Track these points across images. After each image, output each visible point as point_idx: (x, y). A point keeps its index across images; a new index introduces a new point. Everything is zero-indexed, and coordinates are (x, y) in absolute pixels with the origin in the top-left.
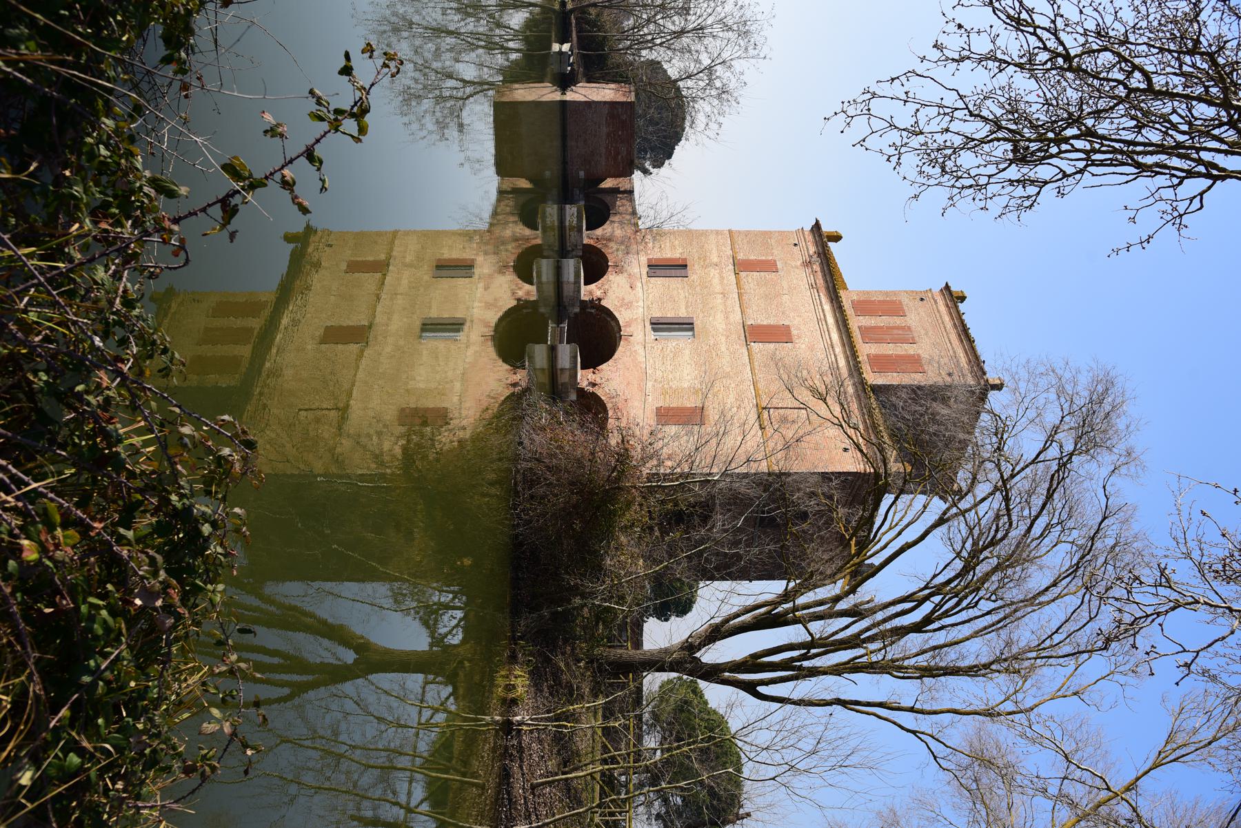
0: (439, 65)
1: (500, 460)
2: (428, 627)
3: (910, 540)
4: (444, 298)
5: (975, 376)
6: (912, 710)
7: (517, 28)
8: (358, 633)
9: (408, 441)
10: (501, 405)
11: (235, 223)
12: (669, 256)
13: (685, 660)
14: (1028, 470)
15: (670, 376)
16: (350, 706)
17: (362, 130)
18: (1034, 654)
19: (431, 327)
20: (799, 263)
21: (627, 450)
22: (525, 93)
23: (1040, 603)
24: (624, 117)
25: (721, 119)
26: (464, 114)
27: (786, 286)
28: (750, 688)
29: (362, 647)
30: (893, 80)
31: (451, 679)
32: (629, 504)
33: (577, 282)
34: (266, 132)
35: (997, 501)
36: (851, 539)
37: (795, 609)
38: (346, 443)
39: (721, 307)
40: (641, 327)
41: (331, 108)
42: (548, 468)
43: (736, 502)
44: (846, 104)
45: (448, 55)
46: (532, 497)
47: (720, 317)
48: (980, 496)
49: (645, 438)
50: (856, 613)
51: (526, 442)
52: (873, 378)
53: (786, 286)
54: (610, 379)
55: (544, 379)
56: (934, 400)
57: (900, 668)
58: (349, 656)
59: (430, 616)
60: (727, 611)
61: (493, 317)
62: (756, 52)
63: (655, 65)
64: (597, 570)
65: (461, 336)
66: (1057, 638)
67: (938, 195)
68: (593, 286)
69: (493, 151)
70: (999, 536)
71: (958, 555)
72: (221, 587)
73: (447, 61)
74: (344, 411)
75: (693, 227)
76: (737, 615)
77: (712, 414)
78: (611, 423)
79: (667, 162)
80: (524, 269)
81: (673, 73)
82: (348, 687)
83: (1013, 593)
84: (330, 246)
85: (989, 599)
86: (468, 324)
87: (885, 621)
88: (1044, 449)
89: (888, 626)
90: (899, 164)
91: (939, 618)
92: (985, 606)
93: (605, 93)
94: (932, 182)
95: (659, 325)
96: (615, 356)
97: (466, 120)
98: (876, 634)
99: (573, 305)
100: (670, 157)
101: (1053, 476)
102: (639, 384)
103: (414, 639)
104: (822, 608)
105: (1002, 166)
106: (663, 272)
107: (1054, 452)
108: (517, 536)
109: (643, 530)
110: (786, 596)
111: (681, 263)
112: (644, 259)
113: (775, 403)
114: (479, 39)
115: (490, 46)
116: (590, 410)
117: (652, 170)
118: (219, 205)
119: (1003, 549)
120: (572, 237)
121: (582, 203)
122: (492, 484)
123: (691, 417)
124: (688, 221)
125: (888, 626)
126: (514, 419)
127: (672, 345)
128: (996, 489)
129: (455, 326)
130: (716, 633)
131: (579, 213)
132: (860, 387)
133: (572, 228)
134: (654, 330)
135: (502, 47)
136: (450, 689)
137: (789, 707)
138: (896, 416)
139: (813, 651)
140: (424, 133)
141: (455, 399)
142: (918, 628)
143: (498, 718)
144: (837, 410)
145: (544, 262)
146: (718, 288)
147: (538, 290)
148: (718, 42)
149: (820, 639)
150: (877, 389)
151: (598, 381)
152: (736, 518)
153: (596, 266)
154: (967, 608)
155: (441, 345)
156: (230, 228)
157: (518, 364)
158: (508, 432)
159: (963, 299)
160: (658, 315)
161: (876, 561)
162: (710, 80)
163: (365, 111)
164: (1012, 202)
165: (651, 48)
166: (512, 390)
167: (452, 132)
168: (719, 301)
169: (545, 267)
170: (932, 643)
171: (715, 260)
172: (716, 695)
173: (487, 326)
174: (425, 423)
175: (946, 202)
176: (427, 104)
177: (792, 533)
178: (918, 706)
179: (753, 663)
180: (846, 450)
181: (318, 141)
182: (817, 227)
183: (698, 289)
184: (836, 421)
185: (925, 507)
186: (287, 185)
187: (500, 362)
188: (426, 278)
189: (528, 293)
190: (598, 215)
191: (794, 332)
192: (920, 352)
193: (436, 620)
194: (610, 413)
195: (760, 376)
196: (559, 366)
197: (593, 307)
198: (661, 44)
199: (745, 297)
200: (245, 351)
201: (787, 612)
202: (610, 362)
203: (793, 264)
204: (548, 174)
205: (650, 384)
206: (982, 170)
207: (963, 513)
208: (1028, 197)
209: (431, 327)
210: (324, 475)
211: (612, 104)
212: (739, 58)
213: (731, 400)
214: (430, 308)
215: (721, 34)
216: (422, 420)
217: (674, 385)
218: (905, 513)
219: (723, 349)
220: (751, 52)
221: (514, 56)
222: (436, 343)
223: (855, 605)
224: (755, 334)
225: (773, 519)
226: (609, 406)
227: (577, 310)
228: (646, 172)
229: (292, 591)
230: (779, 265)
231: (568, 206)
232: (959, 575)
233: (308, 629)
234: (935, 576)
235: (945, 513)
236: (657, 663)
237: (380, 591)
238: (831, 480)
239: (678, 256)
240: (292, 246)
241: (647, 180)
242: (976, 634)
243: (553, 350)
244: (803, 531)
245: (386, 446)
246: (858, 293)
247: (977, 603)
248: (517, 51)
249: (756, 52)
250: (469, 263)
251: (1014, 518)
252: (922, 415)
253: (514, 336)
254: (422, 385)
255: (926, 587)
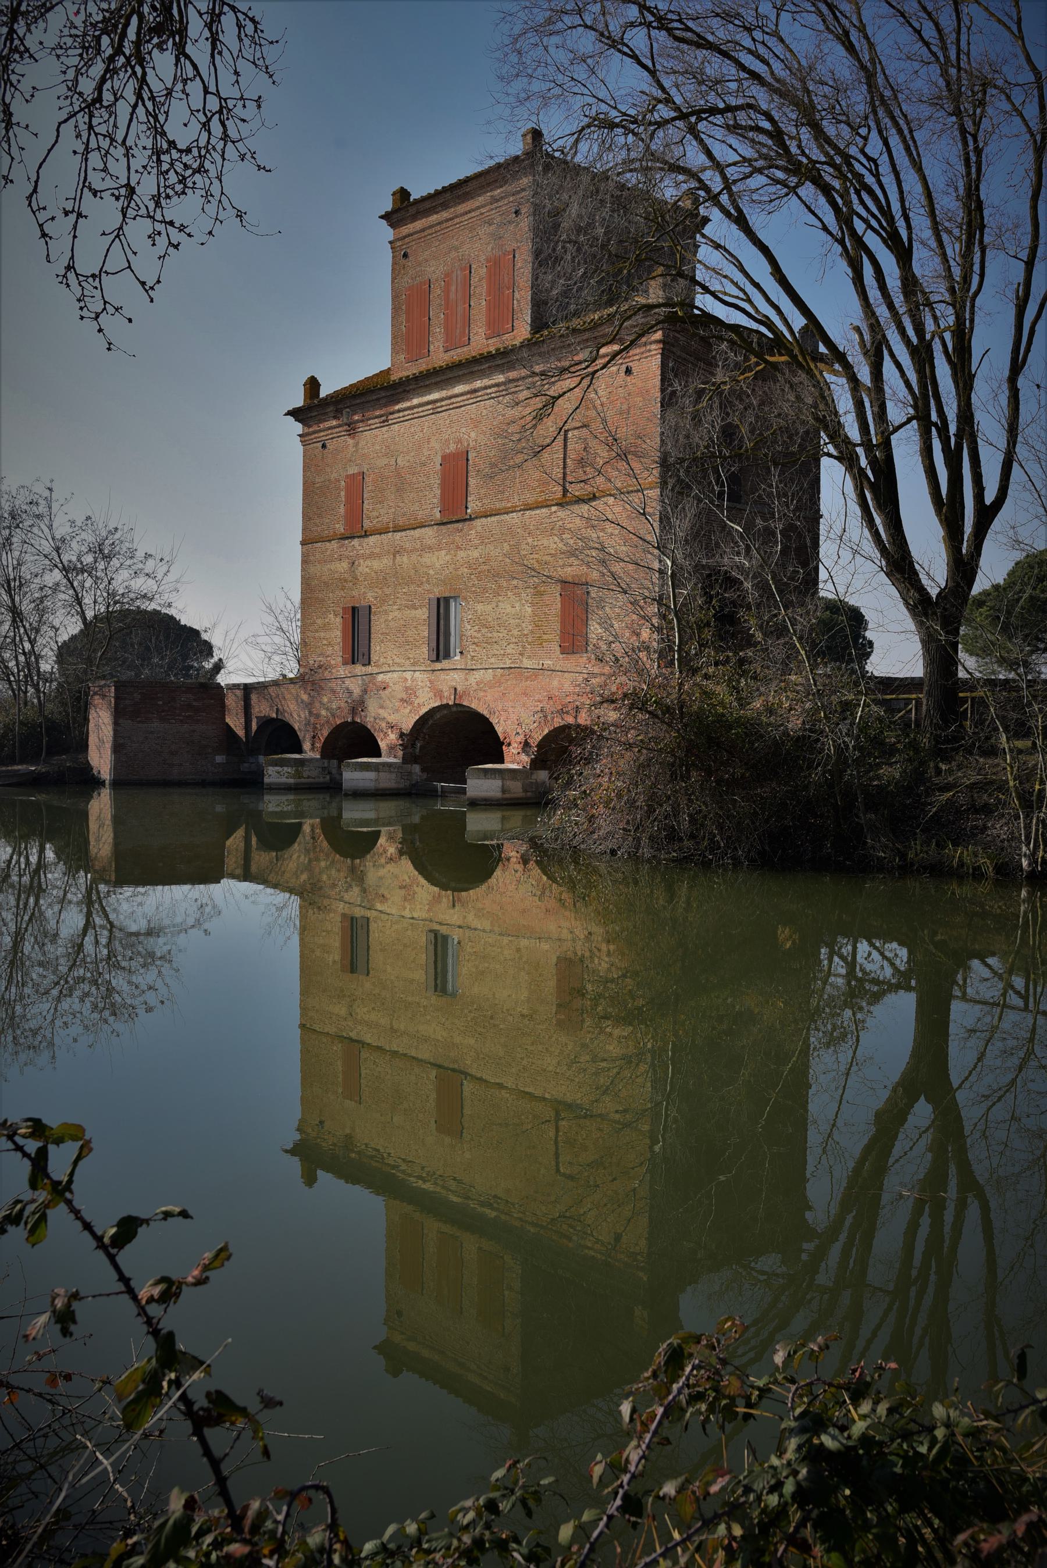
0: (62, 961)
1: (636, 882)
2: (884, 993)
3: (768, 268)
4: (401, 966)
5: (515, 176)
6: (1030, 265)
7: (9, 850)
8: (885, 1095)
9: (606, 1017)
10: (554, 881)
11: (243, 1396)
12: (339, 633)
13: (940, 615)
14: (667, 83)
15: (515, 632)
16: (1000, 1112)
17: (76, 1132)
18: (953, 71)
19: (439, 981)
20: (350, 441)
21: (625, 695)
22: (102, 839)
23: (873, 63)
24: (137, 696)
25: (140, 554)
26: (134, 928)
27: (385, 461)
28: (986, 515)
29: (909, 1089)
30: (44, 235)
31: (961, 959)
32: (707, 694)
33: (376, 768)
34: (66, 1332)
35: (712, 129)
36: (766, 362)
37: (867, 445)
38: (608, 1105)
39: (414, 557)
40: (442, 676)
41: (28, 1195)
42: (651, 810)
43: (705, 534)
44: (85, 313)
45: (49, 947)
46: (692, 837)
47: (428, 559)
48: (702, 159)
49: (607, 670)
50: (876, 352)
51: (610, 844)
52: (523, 331)
53: (385, 461)
54: (517, 722)
55: (516, 818)
56: (556, 226)
57: (966, 279)
58: (922, 1112)
59: (863, 990)
60: (869, 547)
61: (425, 890)
62: (42, 502)
63: (64, 652)
64: (805, 743)
65: (456, 935)
66: (929, 31)
67: (238, 179)
68: (383, 745)
69: (186, 888)
70: (766, 125)
71: (793, 190)
72: (938, 1411)
73: (58, 951)
74: (561, 1108)
75: (297, 597)
76: (876, 535)
77: (571, 570)
78: (583, 719)
79: (205, 636)
80: (357, 845)
81: (72, 627)
82: (970, 1113)
83: (858, 101)
84: (321, 1122)
85: (865, 139)
86: (437, 927)
87: (891, 306)
88: (635, 57)
89: (898, 299)
90: (182, 228)
91: (891, 220)
92: (874, 148)
93: (101, 724)
94: (215, 189)
95: (441, 651)
96: (485, 713)
97: (141, 925)
98: (913, 322)
99: (410, 773)
100: (195, 633)
101: (677, 39)
102: (523, 686)
103: (897, 1016)
104: (867, 404)
105: (190, 72)
106: (363, 641)
107: (638, 39)
108: (752, 861)
109: (745, 674)
110: (848, 458)
111: (349, 616)
112: (342, 671)
113: (558, 473)
114: (26, 904)
115: (36, 889)
116: (565, 750)
117: (215, 659)
118: (207, 1431)
119: (787, 117)
120: (311, 774)
121: (262, 759)
122: (672, 895)
123: (576, 603)
124: (289, 606)
125: (898, 299)
126: (576, 862)
127: (470, 630)
128: (693, 131)
129: (439, 943)
130: (899, 564)
131: (275, 763)
132: (535, 350)
133: (298, 775)
134: (447, 656)
135: (37, 871)
136: (975, 963)
137: (1021, 451)
138: (580, 289)
139: (934, 417)
140: (159, 984)
141: (545, 946)
142: (904, 254)
143: (1024, 893)
144: (569, 383)
145: (347, 815)
146: (387, 561)
147: (389, 824)
148: (28, 557)
149: (915, 407)
150: (539, 324)
151: (521, 738)
152: (730, 532)
153: (354, 739)
154: (877, 175)
155: (466, 969)
156: (253, 1405)
157: (496, 854)
158: (596, 870)
159: (403, 194)
160: (425, 649)
161: (798, 322)
162: (82, 571)
163: (38, 1128)
164: (248, 53)
165: (38, 657)
166: (532, 864)
167: (159, 945)
168: (405, 559)
169: (354, 813)
170: (927, 234)
171: (345, 565)
172: (994, 568)
173: (437, 900)
174: (581, 993)
175: (248, 165)
176: (119, 981)
177: (757, 447)
178: (1024, 255)
179: (949, 510)
180: (628, 371)
181: (87, 1226)
182: (295, 413)
183: (388, 591)
184: (586, 382)
185: (718, 246)
186: (171, 1290)
187: (492, 881)
188: (368, 985)
189: (391, 838)
190: (279, 736)
191: (452, 447)
192: (483, 258)
193: (876, 982)
194: (570, 720)
195: (516, 501)
196: (498, 794)
197: (413, 745)
198: (32, 642)
199: (401, 521)
200: (471, 1245)
201: (873, 462)
202: (494, 720)
203: (352, 449)
204: (219, 808)
205: (527, 663)
206: (197, 102)
207: (728, 186)
208: (240, 26)
209: (439, 981)
210: (654, 1141)
211: (119, 714)
212: (50, 527)
213: (553, 543)
214: (412, 981)
215: (16, 554)
216: (573, 991)
217: (527, 627)
218: (726, 279)
219: (476, 554)
220: (42, 509)
221: (50, 855)
222: (463, 973)
223: (865, 354)
224: (455, 512)
225: (733, 479)
226: (558, 722)
227: (417, 768)
228: (218, 667)
229: (823, 1191)
230: (353, 470)
231: (266, 780)
232: (826, 190)
233: (881, 1170)
234: (825, 228)
235: (727, 214)
236: (941, 657)
237: (824, 1065)
238: (674, 393)
239: (339, 620)
240: (320, 1173)
241: (230, 665)
242: (917, 166)
243: (475, 804)
244: (752, 431)
245: (613, 1049)
246: (395, 351)
247: (869, 159)
248: (42, 851)
249: (42, 502)
250: (347, 924)
251: (740, 101)
252: (579, 250)
253: (458, 864)
254: (524, 995)
255: (841, 242)
